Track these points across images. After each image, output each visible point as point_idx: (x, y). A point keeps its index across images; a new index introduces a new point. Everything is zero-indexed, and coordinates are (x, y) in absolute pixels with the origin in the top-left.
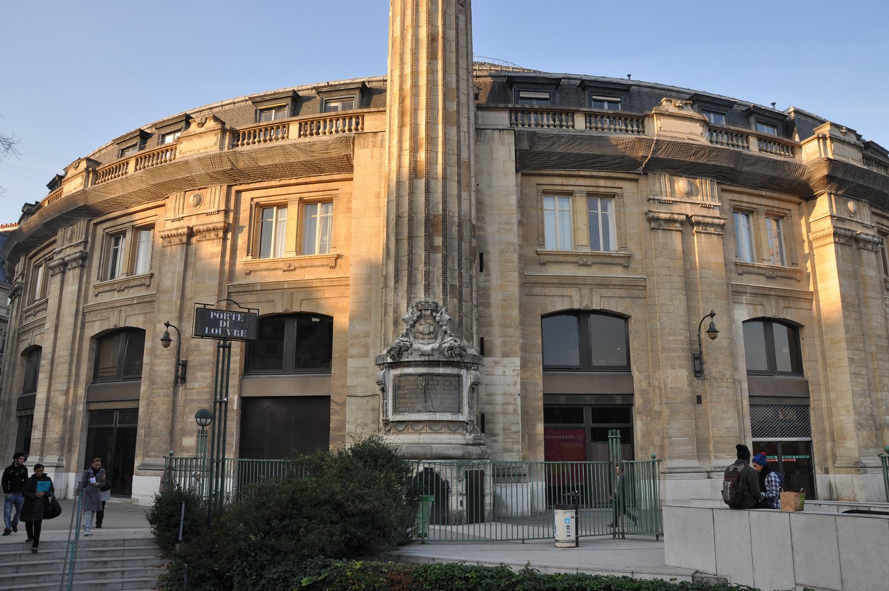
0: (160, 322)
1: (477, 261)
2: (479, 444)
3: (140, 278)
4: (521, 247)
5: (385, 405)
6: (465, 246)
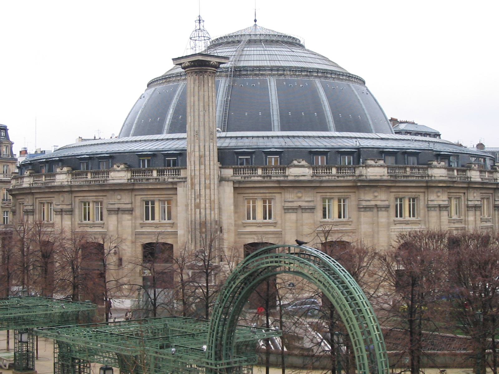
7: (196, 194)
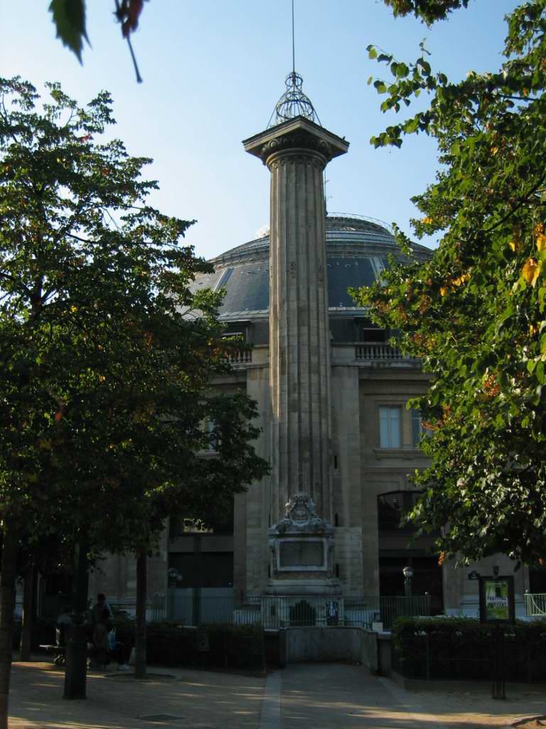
7: (292, 383)
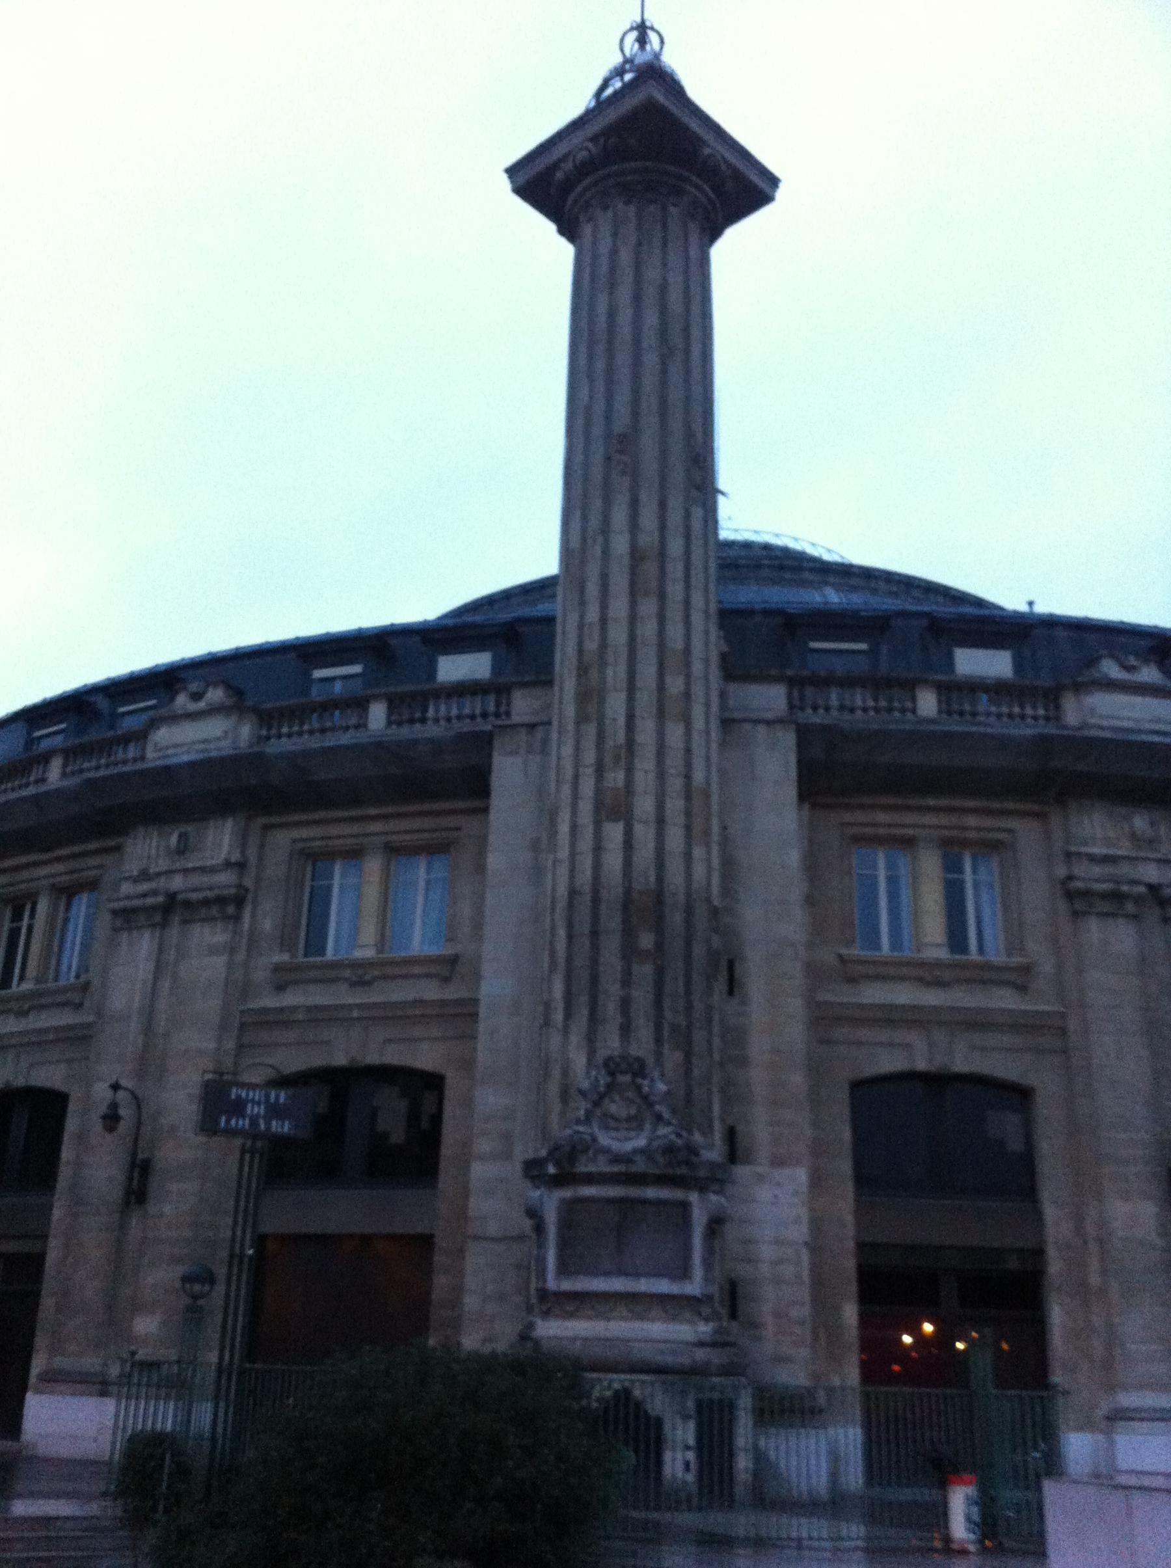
0: (100, 1079)
1: (723, 977)
2: (725, 1344)
3: (64, 990)
4: (810, 946)
5: (541, 1261)
6: (698, 950)
7: (610, 743)
